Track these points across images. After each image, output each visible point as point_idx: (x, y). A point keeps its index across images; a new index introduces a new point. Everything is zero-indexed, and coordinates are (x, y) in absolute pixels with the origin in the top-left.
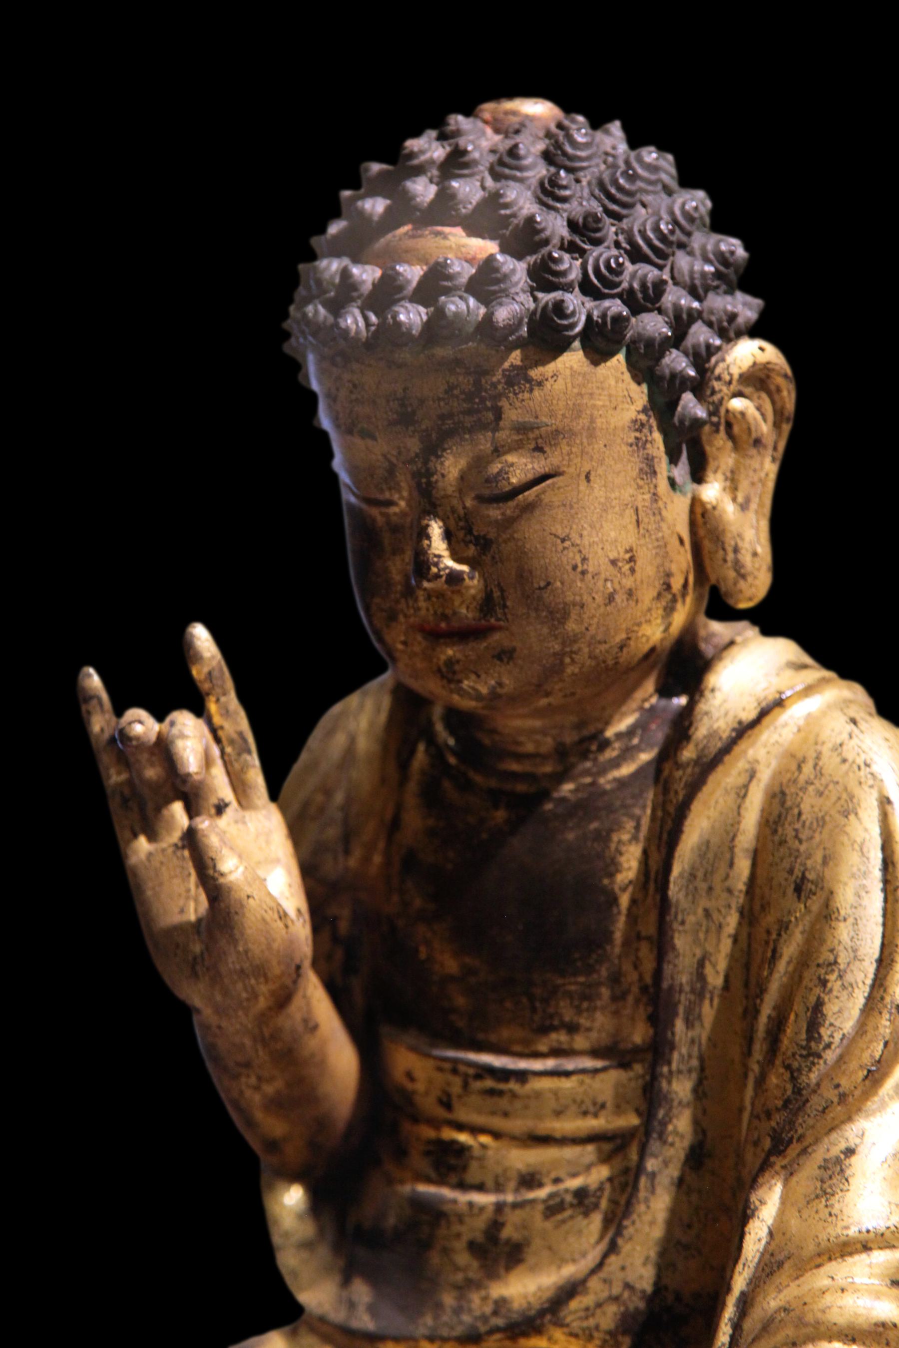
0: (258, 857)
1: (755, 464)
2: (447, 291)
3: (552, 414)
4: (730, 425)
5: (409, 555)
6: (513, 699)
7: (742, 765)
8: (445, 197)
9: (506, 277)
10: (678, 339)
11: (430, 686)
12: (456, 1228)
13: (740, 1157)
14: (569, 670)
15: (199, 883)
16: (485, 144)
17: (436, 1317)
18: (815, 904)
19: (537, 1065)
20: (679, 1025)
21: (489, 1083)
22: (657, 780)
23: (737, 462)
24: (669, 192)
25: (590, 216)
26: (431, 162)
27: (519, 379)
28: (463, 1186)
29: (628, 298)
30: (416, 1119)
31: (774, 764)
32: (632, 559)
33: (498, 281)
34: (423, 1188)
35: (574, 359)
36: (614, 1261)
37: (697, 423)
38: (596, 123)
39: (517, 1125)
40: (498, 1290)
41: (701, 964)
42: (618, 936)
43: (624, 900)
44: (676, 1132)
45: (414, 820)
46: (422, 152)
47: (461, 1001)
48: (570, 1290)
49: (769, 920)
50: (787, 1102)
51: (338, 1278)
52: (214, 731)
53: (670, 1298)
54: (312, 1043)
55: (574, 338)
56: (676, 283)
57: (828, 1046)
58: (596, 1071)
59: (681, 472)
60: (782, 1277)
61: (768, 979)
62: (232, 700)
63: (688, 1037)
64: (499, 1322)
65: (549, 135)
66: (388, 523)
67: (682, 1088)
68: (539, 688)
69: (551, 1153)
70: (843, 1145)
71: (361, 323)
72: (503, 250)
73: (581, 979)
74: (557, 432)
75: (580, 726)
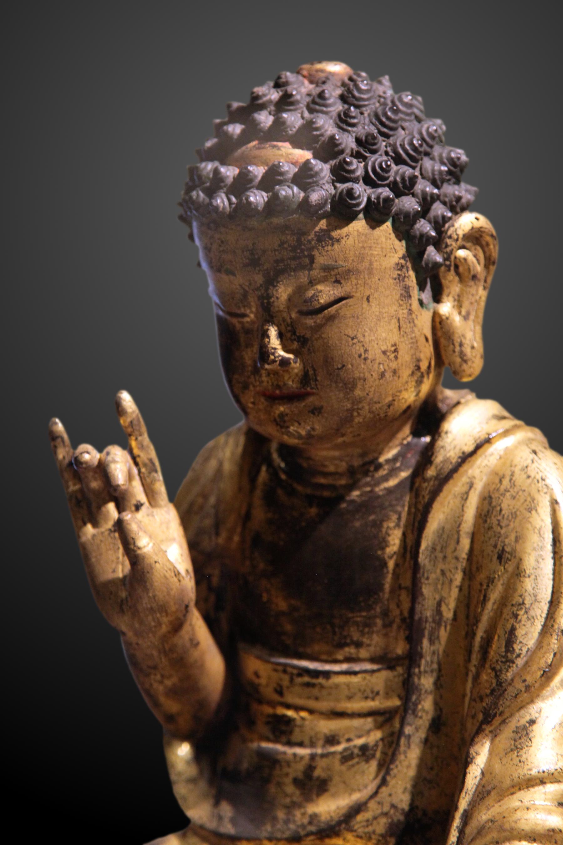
0: (162, 538)
1: (473, 291)
2: (280, 183)
3: (346, 260)
4: (457, 267)
5: (256, 348)
6: (321, 438)
7: (464, 479)
8: (279, 123)
9: (317, 174)
10: (424, 213)
11: (269, 430)
12: (286, 770)
13: (463, 725)
14: (356, 420)
15: (124, 553)
16: (304, 90)
17: (273, 826)
18: (511, 567)
19: (336, 668)
20: (425, 643)
21: (306, 679)
22: (411, 489)
23: (462, 290)
24: (419, 120)
25: (370, 136)
26: (270, 101)
27: (325, 238)
28: (290, 744)
29: (394, 187)
30: (260, 701)
31: (485, 479)
32: (396, 351)
33: (312, 176)
34: (265, 745)
35: (359, 225)
36: (384, 790)
37: (437, 265)
38: (375, 77)
39: (324, 705)
40: (312, 809)
41: (439, 604)
42: (387, 587)
43: (391, 564)
44: (423, 710)
45: (260, 514)
46: (264, 95)
47: (288, 627)
48: (357, 809)
49: (482, 577)
50: (493, 691)
51: (211, 801)
52: (134, 458)
53: (420, 814)
54: (195, 654)
55: (359, 212)
56: (423, 178)
57: (519, 656)
58: (373, 672)
59: (427, 296)
60: (490, 801)
61: (481, 613)
62: (145, 439)
63: (431, 650)
64: (313, 828)
65: (344, 84)
66: (243, 328)
67: (427, 682)
68: (338, 432)
69: (345, 723)
70: (528, 718)
71: (226, 203)
72: (315, 157)
73: (364, 614)
74: (349, 271)
75: (363, 455)
